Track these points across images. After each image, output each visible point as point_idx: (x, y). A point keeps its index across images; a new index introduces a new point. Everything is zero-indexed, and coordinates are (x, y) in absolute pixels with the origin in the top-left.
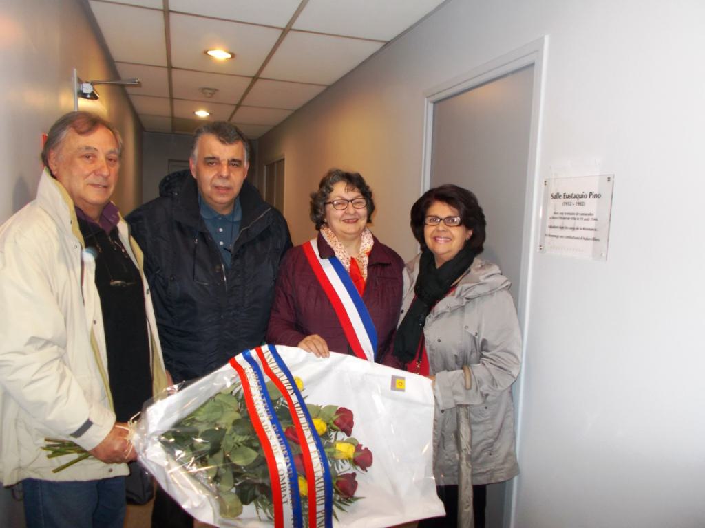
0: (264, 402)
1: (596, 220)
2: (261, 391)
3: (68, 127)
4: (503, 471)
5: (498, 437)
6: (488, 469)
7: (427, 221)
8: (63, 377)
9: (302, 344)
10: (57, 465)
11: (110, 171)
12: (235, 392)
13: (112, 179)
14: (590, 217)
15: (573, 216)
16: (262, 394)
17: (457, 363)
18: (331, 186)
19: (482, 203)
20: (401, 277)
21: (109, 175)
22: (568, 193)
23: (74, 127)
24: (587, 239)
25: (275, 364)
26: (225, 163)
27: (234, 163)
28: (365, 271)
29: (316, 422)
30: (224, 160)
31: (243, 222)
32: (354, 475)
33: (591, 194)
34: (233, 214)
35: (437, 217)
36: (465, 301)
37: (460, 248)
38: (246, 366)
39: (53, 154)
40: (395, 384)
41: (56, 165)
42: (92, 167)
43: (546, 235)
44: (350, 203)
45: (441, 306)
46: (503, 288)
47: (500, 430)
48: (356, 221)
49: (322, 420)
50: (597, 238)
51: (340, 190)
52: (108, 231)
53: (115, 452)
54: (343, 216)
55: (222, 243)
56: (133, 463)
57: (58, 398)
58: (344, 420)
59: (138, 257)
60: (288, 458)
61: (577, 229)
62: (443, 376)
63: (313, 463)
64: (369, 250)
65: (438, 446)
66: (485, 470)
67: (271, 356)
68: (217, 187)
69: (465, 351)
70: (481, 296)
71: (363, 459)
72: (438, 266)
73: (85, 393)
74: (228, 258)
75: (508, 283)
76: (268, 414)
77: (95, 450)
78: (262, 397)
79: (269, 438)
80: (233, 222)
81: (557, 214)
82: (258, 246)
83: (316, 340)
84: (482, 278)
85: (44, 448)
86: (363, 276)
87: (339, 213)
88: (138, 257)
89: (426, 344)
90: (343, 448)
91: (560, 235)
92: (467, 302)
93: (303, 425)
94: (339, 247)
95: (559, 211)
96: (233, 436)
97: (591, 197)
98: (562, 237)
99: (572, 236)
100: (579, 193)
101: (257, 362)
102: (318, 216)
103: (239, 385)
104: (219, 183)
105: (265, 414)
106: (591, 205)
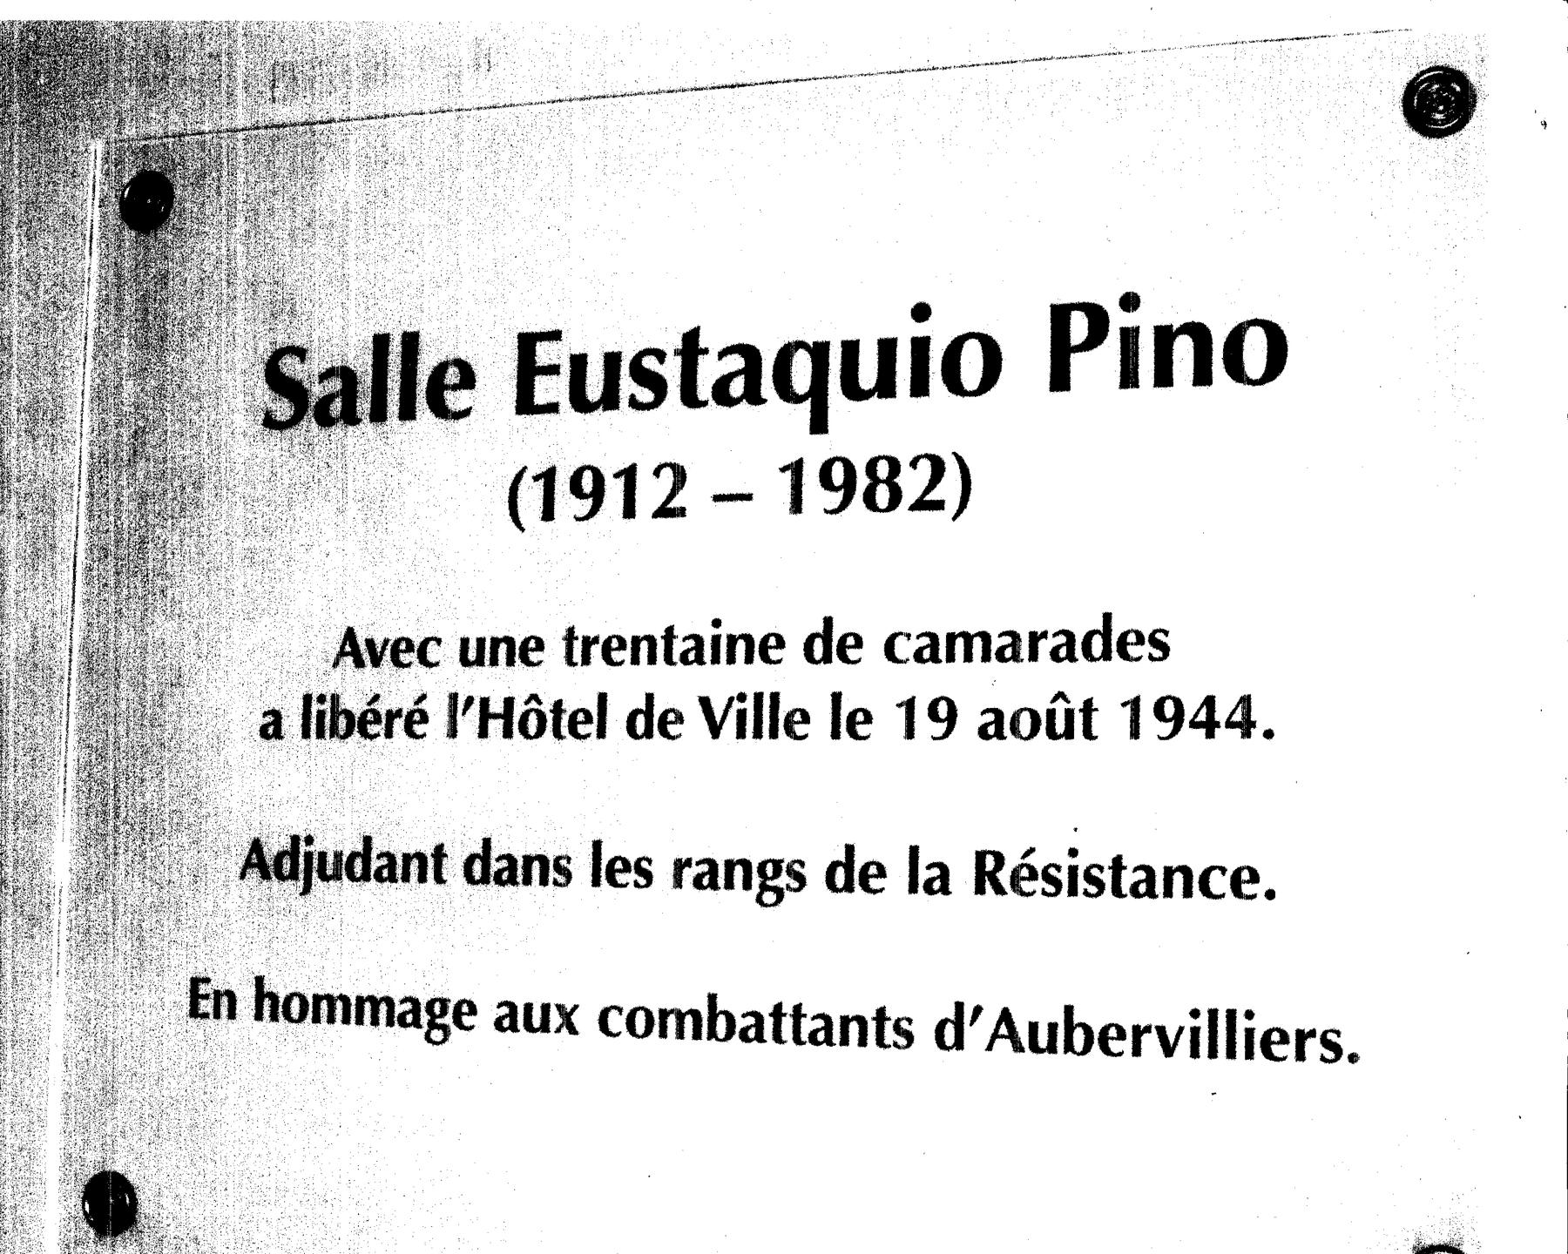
14: (1105, 683)
15: (724, 681)
33: (1071, 331)
43: (208, 1002)
97: (1096, 368)
101: (426, 406)
106: (1067, 498)
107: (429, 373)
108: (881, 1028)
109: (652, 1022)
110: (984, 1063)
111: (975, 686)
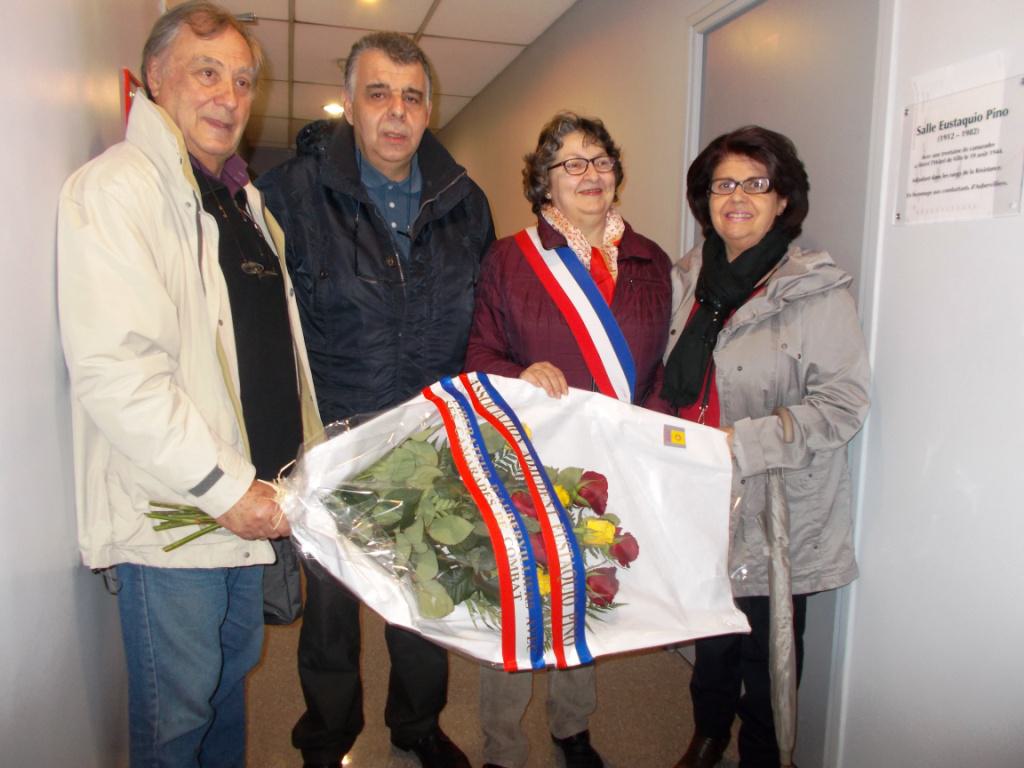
0: (477, 452)
1: (999, 152)
2: (472, 436)
3: (181, 22)
4: (834, 573)
5: (827, 520)
6: (813, 570)
7: (715, 187)
8: (176, 402)
9: (527, 373)
10: (169, 542)
11: (237, 101)
12: (430, 440)
13: (242, 115)
14: (988, 150)
15: (955, 155)
16: (474, 440)
17: (766, 405)
19: (802, 155)
20: (669, 281)
21: (235, 108)
23: (191, 24)
24: (983, 186)
25: (490, 400)
26: (397, 94)
27: (411, 95)
28: (614, 266)
29: (557, 489)
30: (397, 90)
31: (425, 193)
32: (613, 570)
34: (409, 182)
35: (731, 180)
36: (782, 304)
37: (768, 229)
38: (448, 399)
39: (155, 63)
40: (669, 436)
41: (158, 83)
42: (212, 92)
43: (908, 195)
44: (590, 164)
45: (743, 315)
46: (842, 285)
47: (831, 509)
48: (599, 192)
49: (563, 488)
50: (1001, 181)
51: (574, 145)
52: (233, 191)
53: (258, 520)
54: (579, 184)
55: (394, 225)
56: (284, 543)
57: (172, 430)
58: (593, 491)
59: (275, 237)
60: (519, 532)
61: (965, 173)
62: (743, 424)
63: (557, 543)
64: (619, 238)
65: (735, 537)
66: (807, 572)
67: (482, 389)
68: (386, 134)
69: (780, 384)
70: (807, 297)
71: (625, 550)
72: (731, 258)
73: (210, 429)
74: (405, 245)
75: (848, 278)
76: (485, 470)
77: (226, 516)
78: (475, 445)
79: (489, 502)
80: (410, 196)
81: (928, 157)
82: (449, 230)
83: (543, 369)
84: (810, 266)
85: (149, 515)
86: (612, 273)
87: (573, 181)
88: (275, 237)
89: (717, 376)
90: (598, 530)
91: (933, 190)
92: (786, 306)
93: (538, 487)
94: (573, 232)
95: (930, 152)
96: (434, 501)
97: (991, 117)
98: (936, 192)
99: (955, 187)
100: (967, 116)
102: (538, 189)
103: (438, 428)
104: (390, 127)
105: (480, 470)
107: (730, 745)
108: (966, 188)
109: (948, 191)
110: (976, 190)
111: (977, 152)
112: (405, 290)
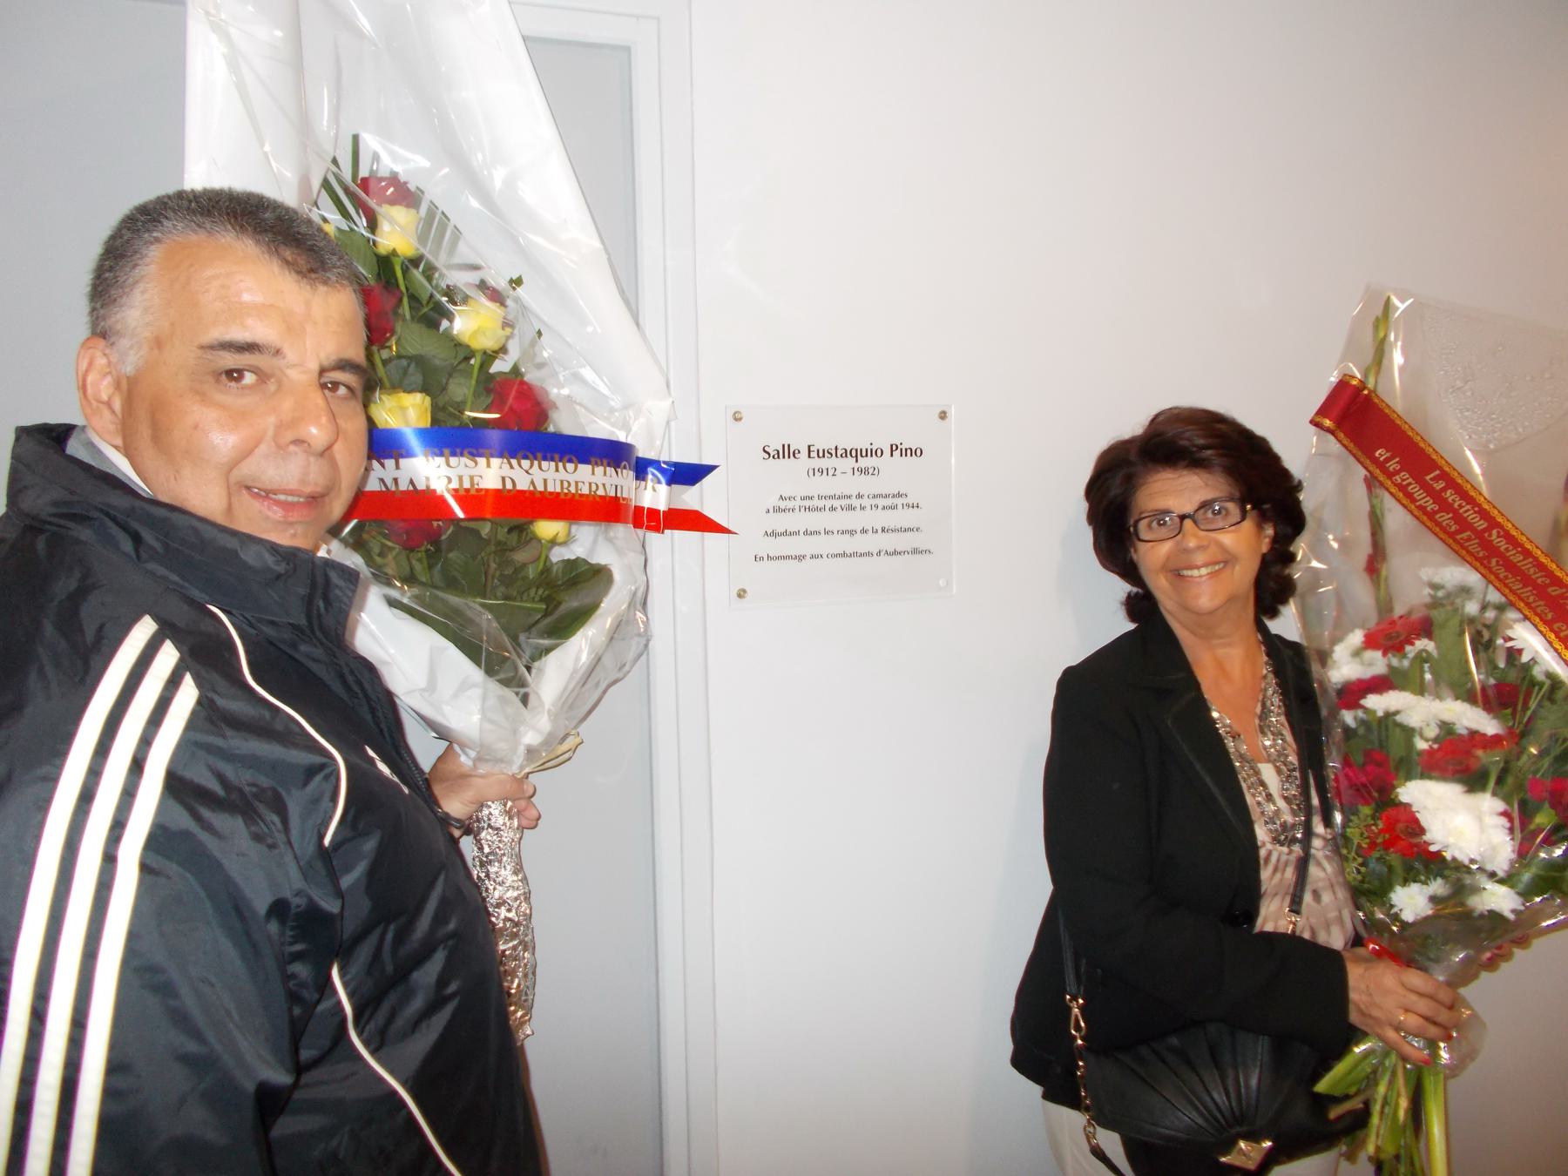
14: (899, 501)
15: (844, 502)
18: (551, 429)
22: (820, 445)
111: (881, 502)
112: (408, 316)
